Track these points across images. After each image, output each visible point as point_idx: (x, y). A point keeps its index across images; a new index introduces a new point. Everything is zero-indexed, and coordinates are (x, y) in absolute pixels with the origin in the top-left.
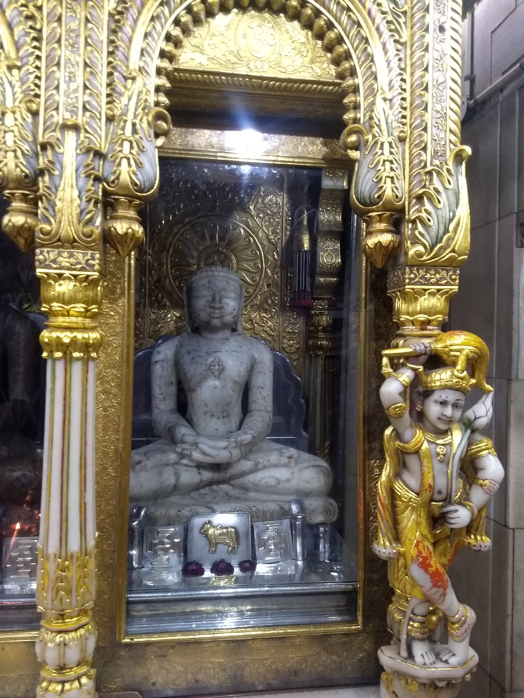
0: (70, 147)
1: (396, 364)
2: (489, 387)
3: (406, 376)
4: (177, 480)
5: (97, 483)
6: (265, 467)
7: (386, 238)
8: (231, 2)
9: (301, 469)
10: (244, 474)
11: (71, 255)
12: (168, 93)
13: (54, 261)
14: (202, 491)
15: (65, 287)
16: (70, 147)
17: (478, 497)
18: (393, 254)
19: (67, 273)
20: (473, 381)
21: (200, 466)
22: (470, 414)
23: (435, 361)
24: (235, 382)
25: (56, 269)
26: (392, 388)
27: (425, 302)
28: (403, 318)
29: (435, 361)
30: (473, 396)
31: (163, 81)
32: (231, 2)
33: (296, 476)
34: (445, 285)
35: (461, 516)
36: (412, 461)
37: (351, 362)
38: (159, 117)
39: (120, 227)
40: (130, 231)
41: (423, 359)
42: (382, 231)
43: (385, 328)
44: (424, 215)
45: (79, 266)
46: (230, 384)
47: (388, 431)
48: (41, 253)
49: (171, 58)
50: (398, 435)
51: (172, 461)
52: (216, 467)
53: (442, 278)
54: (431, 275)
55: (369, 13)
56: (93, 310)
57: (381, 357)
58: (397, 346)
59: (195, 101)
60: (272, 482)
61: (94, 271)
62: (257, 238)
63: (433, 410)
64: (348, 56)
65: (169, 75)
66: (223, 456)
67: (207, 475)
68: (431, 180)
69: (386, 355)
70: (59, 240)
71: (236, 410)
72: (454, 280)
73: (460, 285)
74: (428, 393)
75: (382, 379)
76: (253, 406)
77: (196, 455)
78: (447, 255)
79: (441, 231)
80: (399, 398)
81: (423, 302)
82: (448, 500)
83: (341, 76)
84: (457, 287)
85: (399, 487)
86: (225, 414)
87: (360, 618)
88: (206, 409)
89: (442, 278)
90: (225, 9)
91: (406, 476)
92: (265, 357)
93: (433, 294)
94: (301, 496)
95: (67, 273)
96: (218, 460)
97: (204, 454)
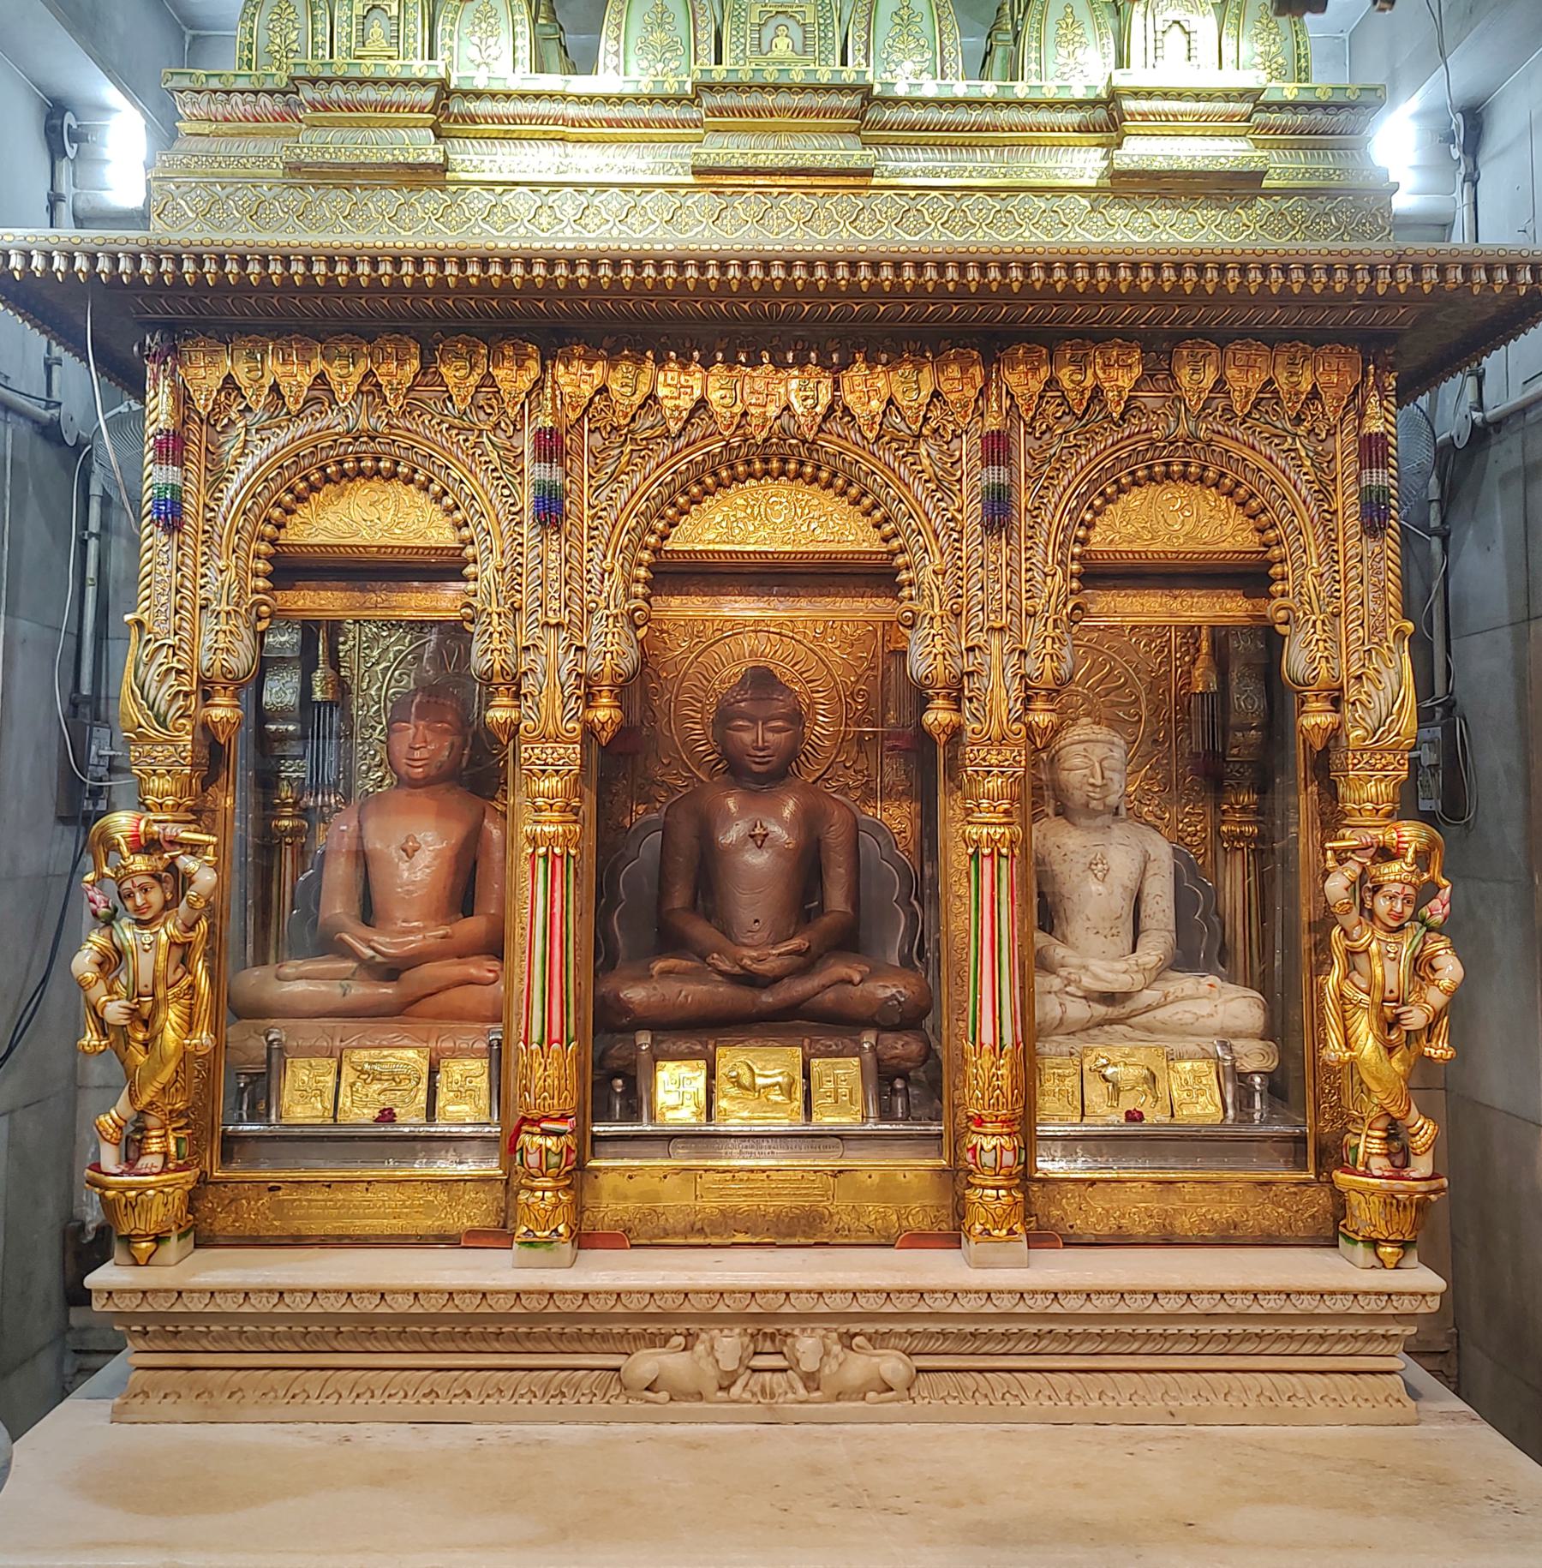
1: (1341, 858)
2: (1445, 882)
3: (1352, 869)
4: (1064, 1012)
6: (1177, 1000)
7: (1325, 720)
9: (1226, 1001)
10: (1149, 1008)
11: (554, 750)
13: (984, 759)
14: (1091, 1032)
15: (993, 784)
17: (1436, 998)
18: (1335, 735)
20: (1426, 876)
21: (1089, 996)
22: (1425, 911)
23: (1386, 854)
24: (1125, 888)
26: (1337, 886)
27: (1371, 789)
28: (1350, 805)
29: (1386, 854)
30: (1427, 892)
33: (1221, 1008)
35: (1416, 1018)
36: (1361, 961)
37: (1068, 905)
39: (217, 714)
41: (1371, 851)
43: (1332, 818)
44: (1363, 697)
46: (1118, 890)
47: (1336, 931)
50: (1346, 933)
51: (1055, 989)
52: (1108, 998)
53: (1388, 764)
55: (1295, 486)
57: (1325, 851)
58: (1343, 838)
60: (1188, 1018)
63: (1382, 905)
66: (1119, 983)
67: (1101, 1010)
68: (1370, 659)
69: (1331, 848)
71: (78, 1347)
74: (1376, 889)
75: (1326, 874)
76: (1146, 923)
77: (1088, 982)
78: (1391, 739)
79: (1396, 688)
80: (1345, 894)
81: (1369, 788)
82: (1400, 1001)
85: (1348, 990)
86: (1114, 931)
87: (1311, 1165)
88: (1088, 924)
89: (1388, 764)
91: (1356, 977)
92: (1161, 850)
93: (161, 776)
94: (1227, 1037)
95: (996, 770)
96: (1115, 987)
97: (1096, 977)
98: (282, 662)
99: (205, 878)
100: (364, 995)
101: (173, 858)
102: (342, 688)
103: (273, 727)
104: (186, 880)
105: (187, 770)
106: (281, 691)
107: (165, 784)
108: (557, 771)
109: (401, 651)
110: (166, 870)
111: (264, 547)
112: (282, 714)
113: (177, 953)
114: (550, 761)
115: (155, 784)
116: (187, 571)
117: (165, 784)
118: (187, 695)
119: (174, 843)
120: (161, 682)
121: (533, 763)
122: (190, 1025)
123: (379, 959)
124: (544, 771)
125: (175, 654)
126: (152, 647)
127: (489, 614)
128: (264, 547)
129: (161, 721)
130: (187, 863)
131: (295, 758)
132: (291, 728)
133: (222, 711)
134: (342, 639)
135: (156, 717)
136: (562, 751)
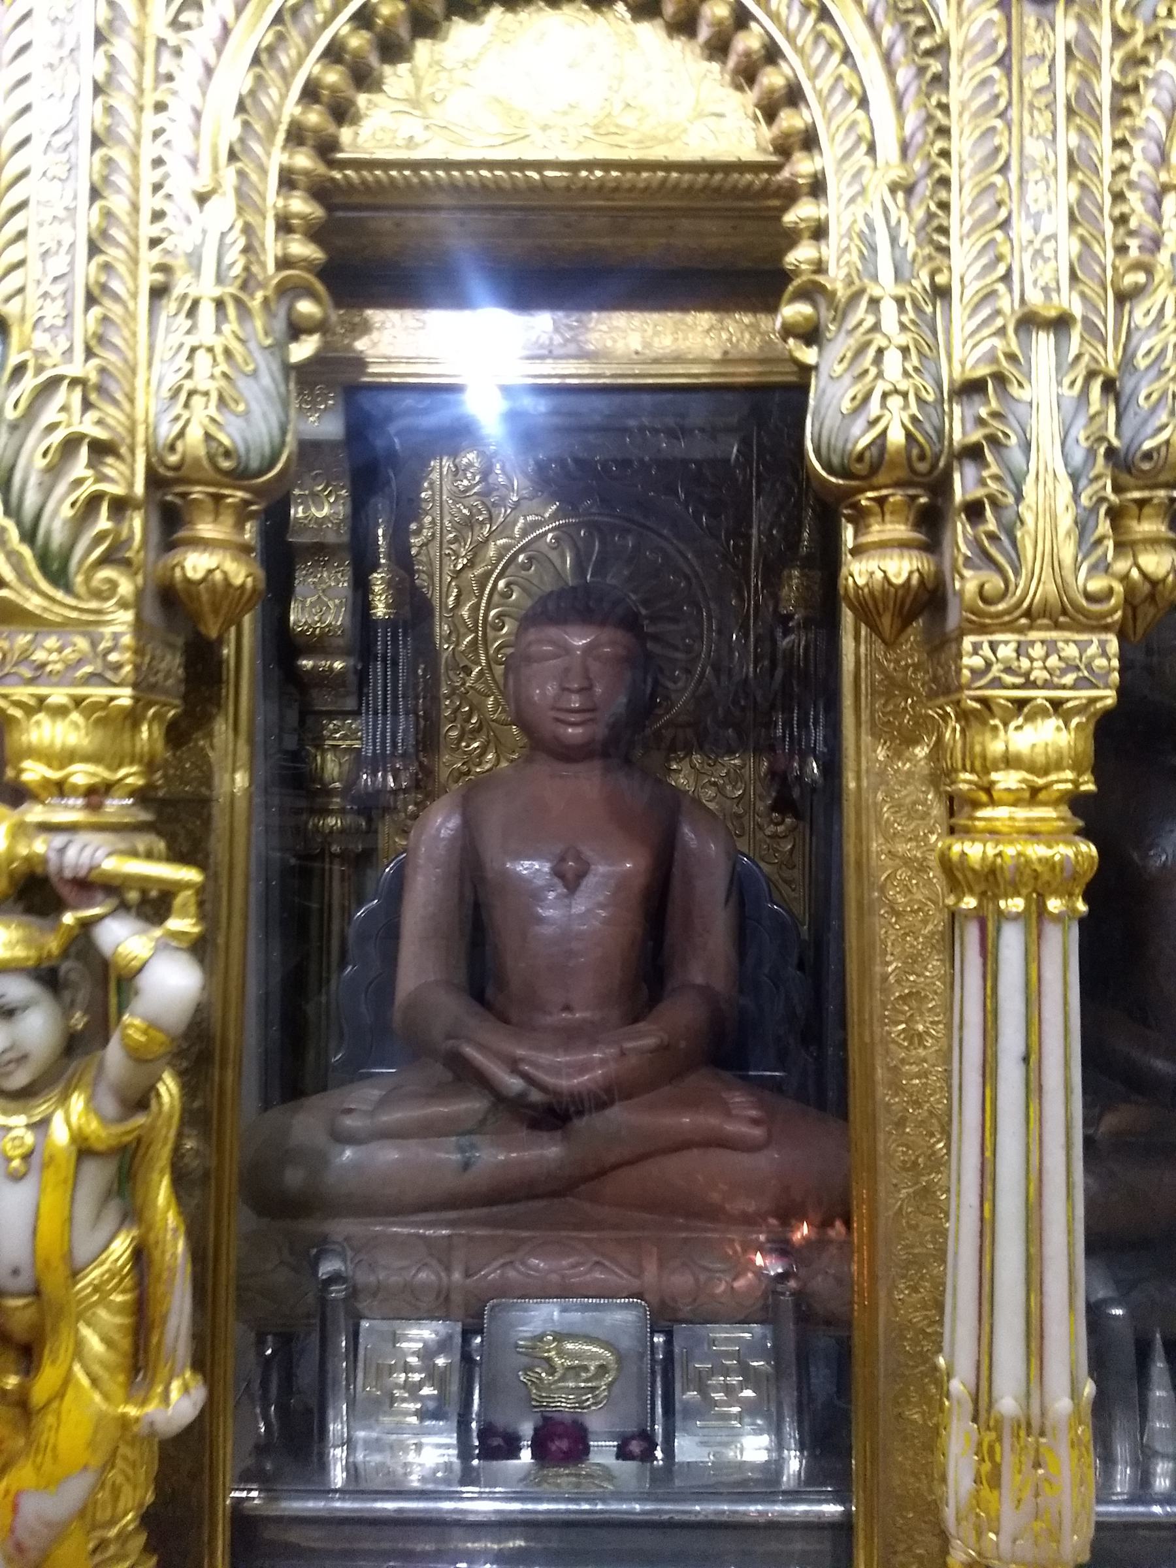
0: (1045, 390)
5: (939, 1286)
8: (438, 8)
11: (1051, 647)
12: (316, 234)
16: (1045, 390)
19: (1040, 696)
25: (1015, 687)
31: (299, 204)
32: (438, 8)
34: (1073, 687)
38: (288, 291)
39: (196, 564)
40: (218, 575)
42: (1153, 542)
45: (1069, 679)
48: (976, 648)
49: (326, 148)
54: (50, 651)
56: (1056, 787)
59: (368, 242)
61: (1107, 687)
62: (492, 572)
64: (794, 96)
65: (320, 192)
70: (1028, 613)
72: (117, 667)
73: (1121, 691)
83: (784, 148)
84: (1111, 693)
90: (425, 25)
93: (60, 712)
98: (320, 552)
99: (169, 981)
100: (505, 1164)
101: (87, 926)
102: (415, 609)
103: (307, 663)
104: (112, 984)
105: (125, 697)
106: (319, 605)
107: (67, 733)
108: (1057, 704)
109: (507, 548)
110: (65, 954)
111: (303, 160)
112: (318, 644)
113: (96, 1175)
114: (1039, 675)
115: (44, 732)
116: (118, 203)
117: (67, 733)
118: (120, 506)
119: (90, 885)
120: (54, 471)
121: (997, 683)
122: (139, 1362)
123: (536, 1096)
124: (1021, 703)
125: (87, 405)
126: (29, 382)
127: (874, 302)
128: (303, 160)
129: (56, 568)
130: (124, 939)
131: (345, 714)
132: (338, 665)
133: (214, 558)
134: (413, 526)
135: (43, 561)
136: (1071, 651)
